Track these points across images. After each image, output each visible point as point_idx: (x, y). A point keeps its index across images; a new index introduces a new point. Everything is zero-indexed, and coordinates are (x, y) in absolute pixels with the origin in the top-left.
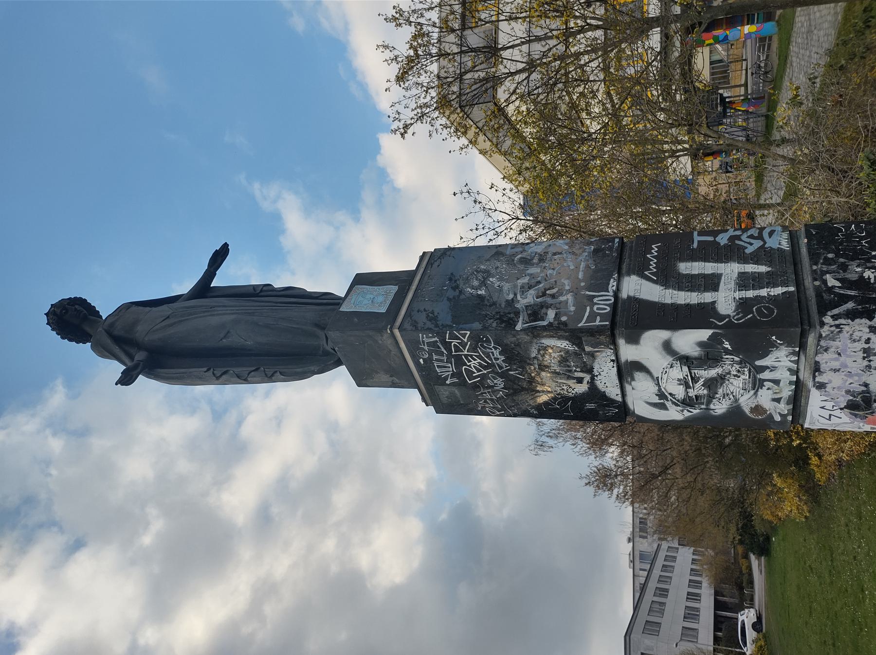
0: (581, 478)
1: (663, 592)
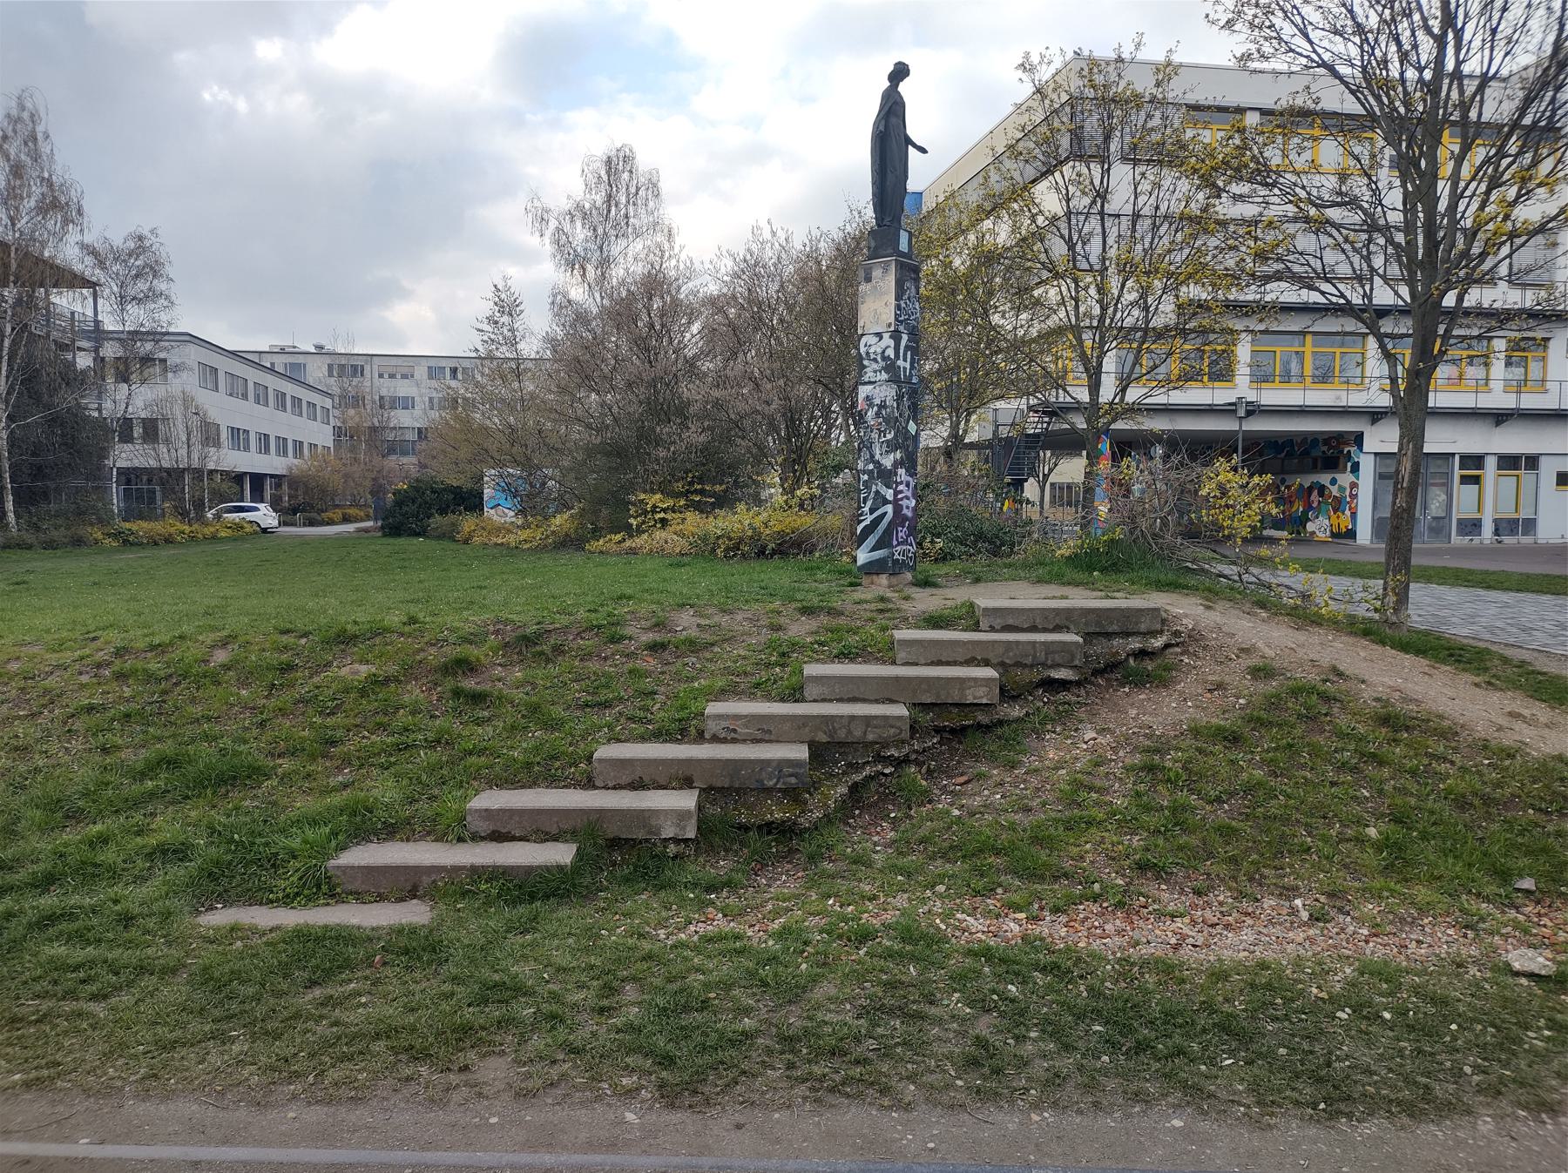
0: (505, 279)
1: (261, 397)
